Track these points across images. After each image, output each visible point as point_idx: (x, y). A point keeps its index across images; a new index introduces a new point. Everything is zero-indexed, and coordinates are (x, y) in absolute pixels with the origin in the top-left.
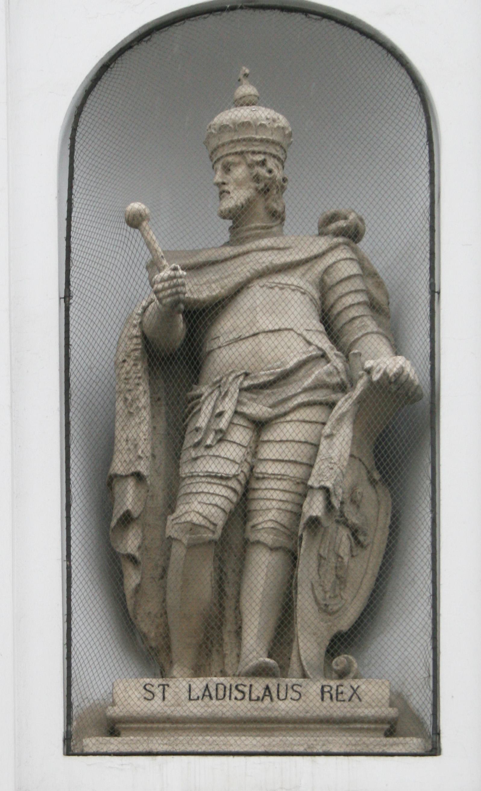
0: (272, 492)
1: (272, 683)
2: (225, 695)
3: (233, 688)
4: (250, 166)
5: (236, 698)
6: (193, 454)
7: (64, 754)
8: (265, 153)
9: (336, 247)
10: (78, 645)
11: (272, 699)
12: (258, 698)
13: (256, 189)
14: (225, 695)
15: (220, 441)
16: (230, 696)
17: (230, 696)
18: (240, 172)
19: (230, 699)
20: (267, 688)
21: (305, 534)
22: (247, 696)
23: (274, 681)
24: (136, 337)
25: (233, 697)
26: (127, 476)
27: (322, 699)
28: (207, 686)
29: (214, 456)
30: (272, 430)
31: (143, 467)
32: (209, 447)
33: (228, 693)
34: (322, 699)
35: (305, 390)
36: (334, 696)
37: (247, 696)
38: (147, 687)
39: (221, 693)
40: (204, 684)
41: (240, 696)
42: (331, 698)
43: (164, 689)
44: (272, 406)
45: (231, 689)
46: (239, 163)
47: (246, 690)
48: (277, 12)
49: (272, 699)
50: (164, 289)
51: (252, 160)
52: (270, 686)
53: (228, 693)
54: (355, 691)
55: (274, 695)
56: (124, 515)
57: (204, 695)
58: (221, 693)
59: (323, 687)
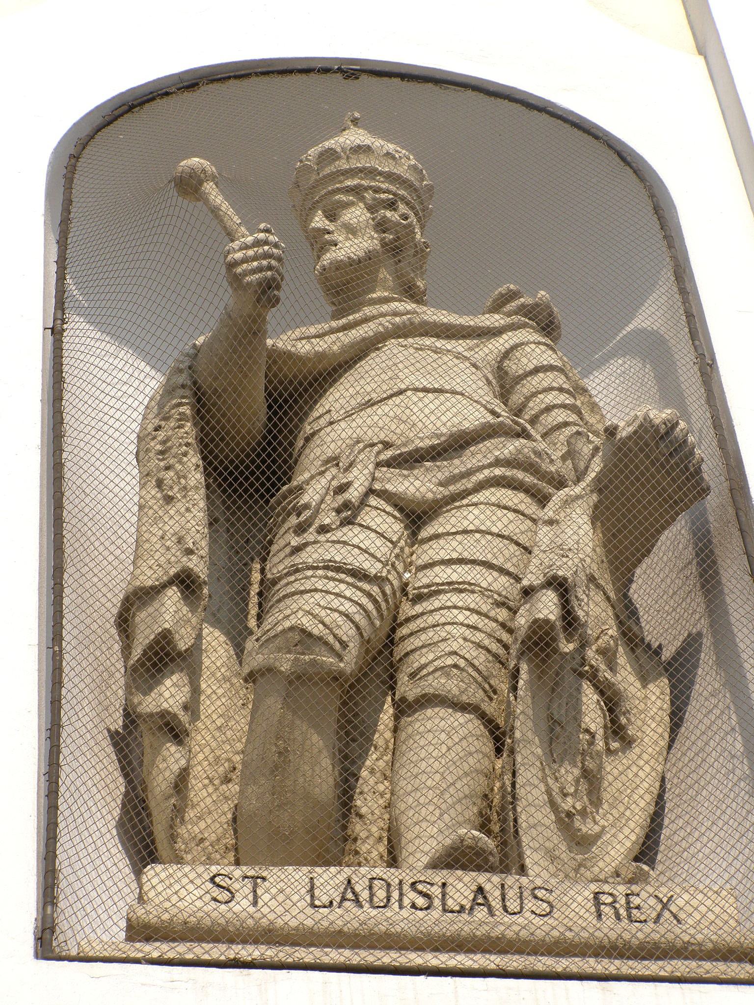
0: (455, 611)
1: (490, 882)
2: (388, 898)
3: (406, 888)
4: (371, 209)
5: (414, 906)
6: (295, 541)
7: (37, 956)
8: (394, 194)
9: (524, 326)
10: (68, 794)
11: (491, 913)
12: (462, 907)
13: (382, 240)
14: (388, 898)
15: (348, 522)
16: (400, 900)
17: (400, 900)
18: (357, 214)
19: (401, 907)
20: (480, 890)
21: (524, 667)
22: (437, 902)
23: (496, 879)
24: (183, 386)
25: (406, 902)
26: (164, 586)
27: (599, 916)
28: (349, 882)
29: (339, 542)
30: (441, 519)
31: (199, 566)
32: (323, 529)
33: (395, 895)
34: (599, 916)
35: (497, 463)
36: (623, 912)
37: (437, 902)
38: (217, 880)
39: (381, 894)
40: (342, 877)
41: (421, 901)
42: (618, 917)
43: (255, 886)
44: (441, 484)
45: (401, 889)
46: (352, 204)
47: (436, 891)
48: (397, 81)
49: (491, 913)
50: (245, 260)
51: (374, 199)
52: (488, 887)
53: (395, 895)
54: (665, 906)
55: (496, 904)
56: (156, 641)
57: (344, 899)
58: (381, 894)
59: (596, 895)
